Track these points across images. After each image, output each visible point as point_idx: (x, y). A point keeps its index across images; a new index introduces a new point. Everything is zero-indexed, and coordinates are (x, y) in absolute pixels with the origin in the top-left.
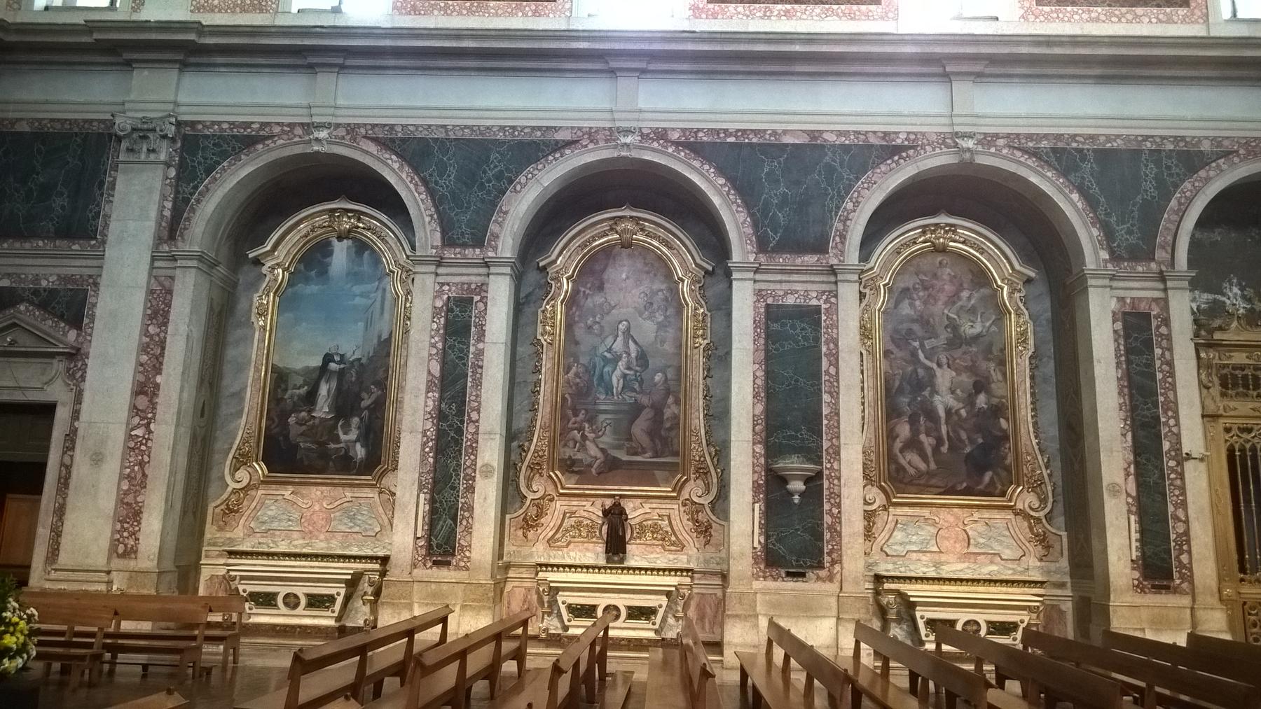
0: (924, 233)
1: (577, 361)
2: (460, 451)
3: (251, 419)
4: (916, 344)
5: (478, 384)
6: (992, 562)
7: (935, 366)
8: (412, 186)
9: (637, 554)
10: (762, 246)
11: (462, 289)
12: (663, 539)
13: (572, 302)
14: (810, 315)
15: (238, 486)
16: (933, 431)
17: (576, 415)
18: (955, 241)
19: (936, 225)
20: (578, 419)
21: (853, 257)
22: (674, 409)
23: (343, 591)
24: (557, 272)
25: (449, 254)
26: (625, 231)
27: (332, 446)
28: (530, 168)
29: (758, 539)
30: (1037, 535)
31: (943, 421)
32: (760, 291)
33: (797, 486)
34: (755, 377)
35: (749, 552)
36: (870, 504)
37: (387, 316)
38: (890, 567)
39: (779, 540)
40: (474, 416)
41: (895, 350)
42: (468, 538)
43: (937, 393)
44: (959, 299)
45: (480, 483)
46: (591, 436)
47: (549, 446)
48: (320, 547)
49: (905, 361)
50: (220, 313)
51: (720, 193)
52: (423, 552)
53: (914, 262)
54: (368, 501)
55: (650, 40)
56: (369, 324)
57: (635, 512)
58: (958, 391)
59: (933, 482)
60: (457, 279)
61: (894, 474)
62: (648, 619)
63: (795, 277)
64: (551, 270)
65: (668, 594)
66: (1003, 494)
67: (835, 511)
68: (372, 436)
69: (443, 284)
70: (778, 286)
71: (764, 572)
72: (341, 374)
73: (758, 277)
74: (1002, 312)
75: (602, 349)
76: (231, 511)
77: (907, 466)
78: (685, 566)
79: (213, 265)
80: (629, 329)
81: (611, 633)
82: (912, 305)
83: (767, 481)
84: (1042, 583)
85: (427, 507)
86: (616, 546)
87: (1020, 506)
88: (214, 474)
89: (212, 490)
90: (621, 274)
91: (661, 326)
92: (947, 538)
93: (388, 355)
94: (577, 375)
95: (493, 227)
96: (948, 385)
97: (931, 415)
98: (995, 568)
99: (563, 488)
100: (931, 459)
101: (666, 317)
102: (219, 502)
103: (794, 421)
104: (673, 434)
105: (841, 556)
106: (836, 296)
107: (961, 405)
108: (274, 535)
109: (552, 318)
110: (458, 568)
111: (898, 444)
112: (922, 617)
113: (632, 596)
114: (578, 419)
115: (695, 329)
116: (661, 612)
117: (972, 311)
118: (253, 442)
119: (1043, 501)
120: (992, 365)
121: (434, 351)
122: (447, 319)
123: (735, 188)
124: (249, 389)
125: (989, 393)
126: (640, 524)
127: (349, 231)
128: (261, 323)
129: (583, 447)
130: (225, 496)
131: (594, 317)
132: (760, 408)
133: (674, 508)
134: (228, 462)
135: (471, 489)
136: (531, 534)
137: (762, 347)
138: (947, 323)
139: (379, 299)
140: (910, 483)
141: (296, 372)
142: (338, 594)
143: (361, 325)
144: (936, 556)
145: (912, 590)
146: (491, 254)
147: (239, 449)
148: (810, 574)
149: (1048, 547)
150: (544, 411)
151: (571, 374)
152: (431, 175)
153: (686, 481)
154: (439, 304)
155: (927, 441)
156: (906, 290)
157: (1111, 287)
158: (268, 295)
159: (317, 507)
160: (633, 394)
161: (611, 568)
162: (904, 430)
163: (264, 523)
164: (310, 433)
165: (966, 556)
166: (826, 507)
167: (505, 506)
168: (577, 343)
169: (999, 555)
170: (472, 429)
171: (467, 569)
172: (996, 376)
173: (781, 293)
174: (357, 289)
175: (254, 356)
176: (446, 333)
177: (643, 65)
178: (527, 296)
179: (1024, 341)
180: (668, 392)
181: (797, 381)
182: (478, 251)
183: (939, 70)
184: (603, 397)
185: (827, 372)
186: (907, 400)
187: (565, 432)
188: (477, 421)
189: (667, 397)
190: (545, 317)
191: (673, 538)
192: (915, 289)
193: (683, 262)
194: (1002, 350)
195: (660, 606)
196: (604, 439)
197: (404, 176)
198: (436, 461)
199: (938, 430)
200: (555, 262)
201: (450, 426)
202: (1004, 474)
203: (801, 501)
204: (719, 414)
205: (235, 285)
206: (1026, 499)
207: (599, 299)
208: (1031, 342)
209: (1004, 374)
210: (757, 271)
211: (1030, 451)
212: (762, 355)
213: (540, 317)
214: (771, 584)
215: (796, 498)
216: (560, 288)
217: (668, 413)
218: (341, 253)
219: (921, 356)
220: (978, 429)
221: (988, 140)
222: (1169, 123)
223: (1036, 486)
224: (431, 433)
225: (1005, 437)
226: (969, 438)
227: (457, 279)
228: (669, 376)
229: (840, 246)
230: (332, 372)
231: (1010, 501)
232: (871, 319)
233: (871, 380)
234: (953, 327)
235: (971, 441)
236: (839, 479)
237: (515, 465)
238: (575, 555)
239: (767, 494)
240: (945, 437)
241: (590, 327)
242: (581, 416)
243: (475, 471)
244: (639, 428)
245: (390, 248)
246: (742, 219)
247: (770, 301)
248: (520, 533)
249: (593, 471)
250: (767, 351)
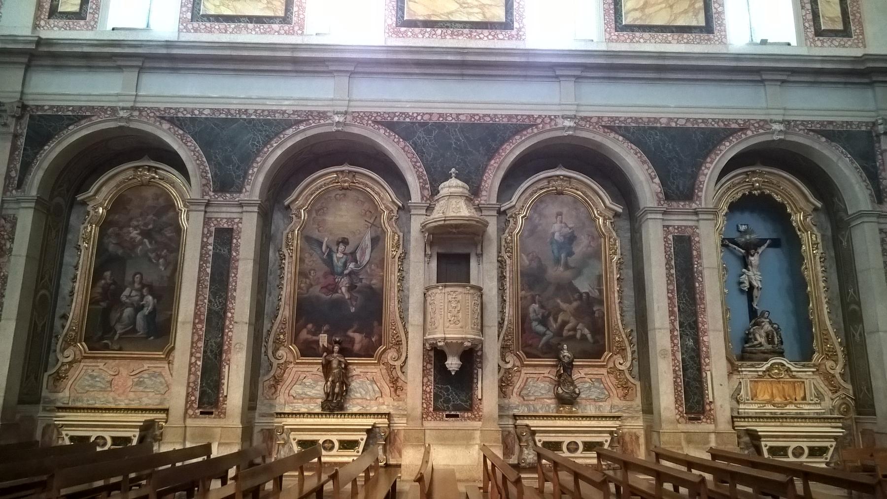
55: (374, 51)
64: (294, 207)
76: (61, 378)
81: (323, 459)
112: (540, 441)
157: (879, 223)
177: (784, 78)
183: (551, 74)
221: (360, 117)
222: (424, 105)
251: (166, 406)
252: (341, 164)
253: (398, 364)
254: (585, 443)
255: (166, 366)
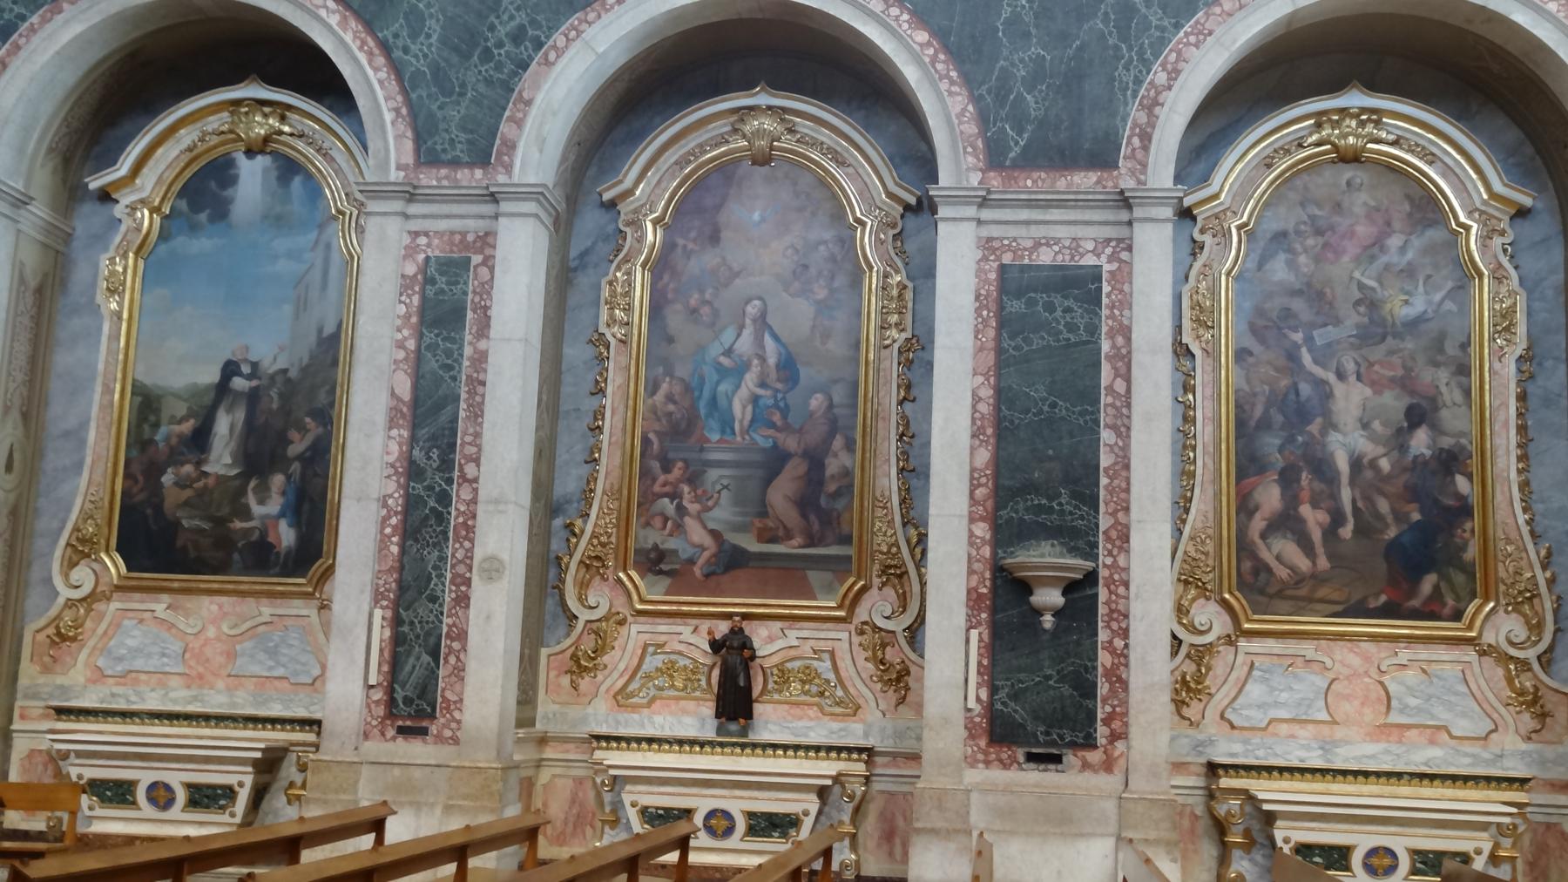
0: (1319, 126)
1: (669, 373)
2: (445, 533)
3: (98, 478)
4: (1298, 337)
5: (477, 413)
6: (1432, 742)
7: (1331, 377)
8: (363, 58)
9: (771, 721)
10: (995, 157)
11: (452, 244)
12: (822, 694)
13: (661, 266)
14: (1080, 286)
15: (77, 594)
16: (1326, 496)
17: (667, 469)
18: (1378, 141)
19: (1343, 111)
20: (672, 477)
21: (1162, 172)
22: (845, 459)
23: (249, 780)
24: (636, 211)
25: (429, 179)
26: (759, 133)
27: (238, 524)
28: (574, 20)
29: (976, 694)
30: (1521, 693)
31: (1345, 479)
32: (990, 240)
33: (1050, 597)
34: (976, 399)
35: (959, 718)
36: (1202, 633)
37: (332, 293)
38: (1237, 748)
39: (1015, 696)
40: (470, 470)
41: (1256, 348)
42: (457, 687)
43: (1335, 427)
44: (1383, 249)
45: (478, 590)
46: (693, 508)
47: (617, 526)
48: (216, 703)
49: (1277, 369)
50: (39, 291)
51: (917, 59)
52: (380, 711)
53: (1298, 182)
54: (300, 621)
56: (301, 306)
57: (768, 642)
58: (1376, 425)
59: (1322, 593)
60: (443, 225)
61: (1249, 579)
62: (784, 835)
63: (1055, 214)
64: (625, 208)
65: (822, 792)
66: (1457, 616)
67: (1119, 643)
68: (306, 507)
69: (416, 234)
70: (1020, 231)
71: (986, 753)
72: (253, 397)
73: (986, 214)
74: (1466, 274)
75: (715, 350)
76: (64, 638)
77: (1273, 564)
78: (862, 743)
79: (21, 202)
80: (763, 315)
81: (694, 858)
82: (1292, 265)
83: (994, 589)
84: (1523, 781)
85: (387, 633)
86: (735, 704)
87: (1489, 638)
88: (36, 574)
89: (33, 600)
90: (753, 211)
91: (822, 307)
92: (1347, 698)
93: (335, 363)
94: (670, 398)
95: (505, 128)
96: (1355, 412)
97: (1322, 467)
98: (1435, 752)
99: (642, 601)
100: (1320, 550)
101: (832, 291)
102: (42, 622)
103: (1049, 479)
104: (840, 504)
105: (1126, 724)
106: (1130, 249)
107: (1381, 450)
108: (136, 682)
109: (627, 294)
110: (440, 739)
111: (1258, 524)
112: (1286, 841)
113: (756, 794)
114: (672, 477)
115: (884, 312)
116: (808, 823)
117: (1409, 272)
118: (101, 517)
119: (1536, 628)
120: (1443, 375)
121: (401, 355)
122: (424, 299)
123: (946, 48)
124: (93, 425)
125: (1436, 429)
126: (780, 667)
127: (267, 140)
128: (114, 306)
129: (679, 528)
130: (53, 612)
131: (702, 292)
132: (984, 456)
133: (841, 638)
134: (58, 553)
135: (463, 600)
136: (585, 683)
137: (991, 344)
138: (1357, 295)
139: (319, 263)
140: (1280, 595)
141: (177, 396)
142: (241, 784)
143: (288, 309)
144: (1326, 730)
145: (1268, 791)
146: (502, 179)
147: (76, 529)
148: (1070, 758)
149: (1543, 716)
150: (610, 462)
151: (659, 397)
152: (396, 36)
153: (864, 589)
154: (410, 269)
155: (1313, 518)
156: (1281, 236)
157: (406, 216)
158: (125, 256)
159: (211, 632)
160: (771, 432)
161: (722, 745)
162: (1270, 497)
163: (120, 659)
164: (202, 501)
165: (1385, 730)
166: (1103, 636)
167: (533, 636)
168: (670, 340)
169: (1446, 729)
170: (466, 494)
171: (456, 741)
172: (1450, 394)
173: (1029, 244)
174: (282, 244)
175: (101, 367)
176: (422, 321)
178: (584, 254)
179: (1507, 329)
180: (833, 428)
181: (1053, 405)
182: (478, 173)
184: (715, 437)
185: (1110, 389)
186: (1277, 442)
187: (648, 499)
188: (476, 480)
189: (832, 434)
190: (613, 294)
191: (840, 693)
192: (1298, 233)
193: (865, 191)
194: (1465, 346)
195: (806, 813)
196: (717, 513)
197: (348, 38)
198: (403, 550)
199: (1335, 496)
200: (629, 192)
201: (430, 488)
202: (1459, 578)
203: (1057, 626)
204: (914, 472)
205: (68, 238)
206: (1505, 628)
207: (710, 259)
208: (1521, 329)
209: (1467, 392)
210: (984, 203)
211: (1514, 535)
212: (990, 359)
213: (606, 292)
214: (998, 775)
215: (1048, 621)
216: (641, 240)
217: (832, 467)
218: (252, 175)
219: (1307, 358)
220: (1413, 494)
223: (1524, 600)
224: (396, 503)
225: (1464, 510)
226: (1394, 511)
227: (443, 225)
228: (836, 399)
229: (1139, 154)
230: (238, 394)
231: (1470, 627)
232: (1214, 291)
233: (1209, 404)
234: (1370, 303)
235: (1399, 517)
236: (1126, 585)
237: (558, 559)
238: (661, 722)
239: (994, 611)
240: (1348, 509)
241: (694, 311)
242: (677, 472)
243: (470, 569)
244: (781, 494)
245: (339, 171)
246: (958, 109)
247: (1007, 259)
248: (566, 680)
249: (697, 571)
250: (999, 351)
251: (317, 716)
252: (746, 85)
253: (898, 626)
254: (1415, 853)
255: (314, 613)
